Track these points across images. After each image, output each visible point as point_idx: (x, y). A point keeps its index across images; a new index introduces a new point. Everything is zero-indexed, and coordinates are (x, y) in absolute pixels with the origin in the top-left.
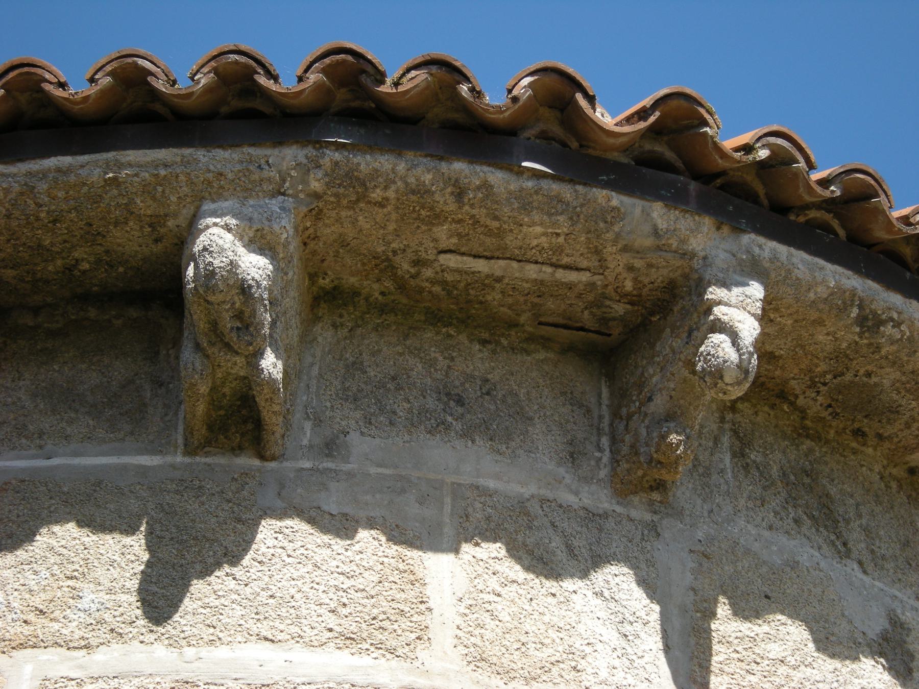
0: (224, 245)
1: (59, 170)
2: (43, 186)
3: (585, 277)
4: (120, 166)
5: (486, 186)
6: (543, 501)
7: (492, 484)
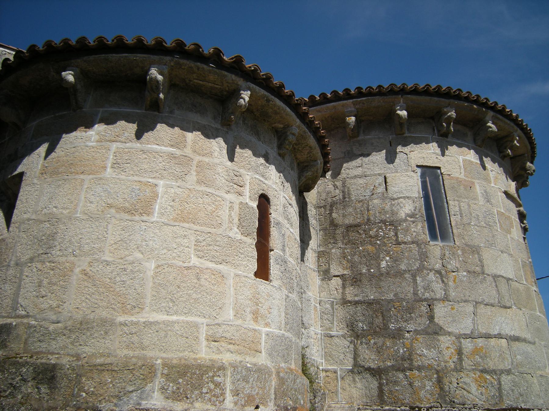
0: (69, 76)
1: (125, 56)
2: (122, 59)
3: (219, 87)
4: (137, 57)
5: (203, 68)
6: (209, 126)
7: (199, 122)
